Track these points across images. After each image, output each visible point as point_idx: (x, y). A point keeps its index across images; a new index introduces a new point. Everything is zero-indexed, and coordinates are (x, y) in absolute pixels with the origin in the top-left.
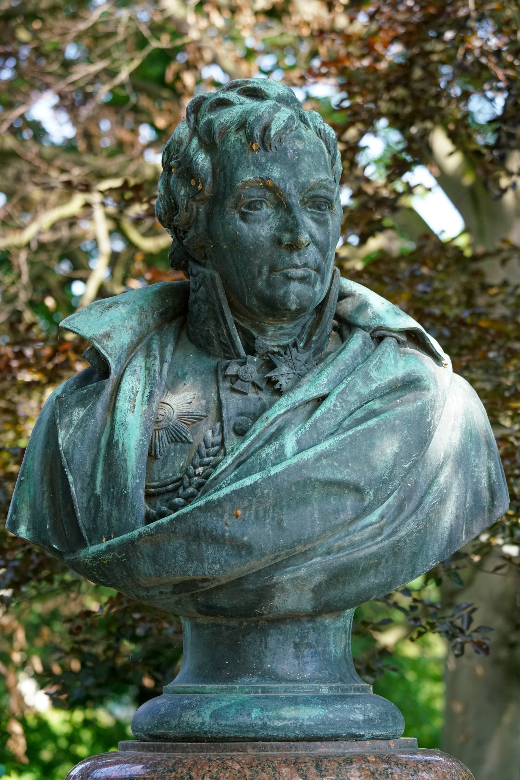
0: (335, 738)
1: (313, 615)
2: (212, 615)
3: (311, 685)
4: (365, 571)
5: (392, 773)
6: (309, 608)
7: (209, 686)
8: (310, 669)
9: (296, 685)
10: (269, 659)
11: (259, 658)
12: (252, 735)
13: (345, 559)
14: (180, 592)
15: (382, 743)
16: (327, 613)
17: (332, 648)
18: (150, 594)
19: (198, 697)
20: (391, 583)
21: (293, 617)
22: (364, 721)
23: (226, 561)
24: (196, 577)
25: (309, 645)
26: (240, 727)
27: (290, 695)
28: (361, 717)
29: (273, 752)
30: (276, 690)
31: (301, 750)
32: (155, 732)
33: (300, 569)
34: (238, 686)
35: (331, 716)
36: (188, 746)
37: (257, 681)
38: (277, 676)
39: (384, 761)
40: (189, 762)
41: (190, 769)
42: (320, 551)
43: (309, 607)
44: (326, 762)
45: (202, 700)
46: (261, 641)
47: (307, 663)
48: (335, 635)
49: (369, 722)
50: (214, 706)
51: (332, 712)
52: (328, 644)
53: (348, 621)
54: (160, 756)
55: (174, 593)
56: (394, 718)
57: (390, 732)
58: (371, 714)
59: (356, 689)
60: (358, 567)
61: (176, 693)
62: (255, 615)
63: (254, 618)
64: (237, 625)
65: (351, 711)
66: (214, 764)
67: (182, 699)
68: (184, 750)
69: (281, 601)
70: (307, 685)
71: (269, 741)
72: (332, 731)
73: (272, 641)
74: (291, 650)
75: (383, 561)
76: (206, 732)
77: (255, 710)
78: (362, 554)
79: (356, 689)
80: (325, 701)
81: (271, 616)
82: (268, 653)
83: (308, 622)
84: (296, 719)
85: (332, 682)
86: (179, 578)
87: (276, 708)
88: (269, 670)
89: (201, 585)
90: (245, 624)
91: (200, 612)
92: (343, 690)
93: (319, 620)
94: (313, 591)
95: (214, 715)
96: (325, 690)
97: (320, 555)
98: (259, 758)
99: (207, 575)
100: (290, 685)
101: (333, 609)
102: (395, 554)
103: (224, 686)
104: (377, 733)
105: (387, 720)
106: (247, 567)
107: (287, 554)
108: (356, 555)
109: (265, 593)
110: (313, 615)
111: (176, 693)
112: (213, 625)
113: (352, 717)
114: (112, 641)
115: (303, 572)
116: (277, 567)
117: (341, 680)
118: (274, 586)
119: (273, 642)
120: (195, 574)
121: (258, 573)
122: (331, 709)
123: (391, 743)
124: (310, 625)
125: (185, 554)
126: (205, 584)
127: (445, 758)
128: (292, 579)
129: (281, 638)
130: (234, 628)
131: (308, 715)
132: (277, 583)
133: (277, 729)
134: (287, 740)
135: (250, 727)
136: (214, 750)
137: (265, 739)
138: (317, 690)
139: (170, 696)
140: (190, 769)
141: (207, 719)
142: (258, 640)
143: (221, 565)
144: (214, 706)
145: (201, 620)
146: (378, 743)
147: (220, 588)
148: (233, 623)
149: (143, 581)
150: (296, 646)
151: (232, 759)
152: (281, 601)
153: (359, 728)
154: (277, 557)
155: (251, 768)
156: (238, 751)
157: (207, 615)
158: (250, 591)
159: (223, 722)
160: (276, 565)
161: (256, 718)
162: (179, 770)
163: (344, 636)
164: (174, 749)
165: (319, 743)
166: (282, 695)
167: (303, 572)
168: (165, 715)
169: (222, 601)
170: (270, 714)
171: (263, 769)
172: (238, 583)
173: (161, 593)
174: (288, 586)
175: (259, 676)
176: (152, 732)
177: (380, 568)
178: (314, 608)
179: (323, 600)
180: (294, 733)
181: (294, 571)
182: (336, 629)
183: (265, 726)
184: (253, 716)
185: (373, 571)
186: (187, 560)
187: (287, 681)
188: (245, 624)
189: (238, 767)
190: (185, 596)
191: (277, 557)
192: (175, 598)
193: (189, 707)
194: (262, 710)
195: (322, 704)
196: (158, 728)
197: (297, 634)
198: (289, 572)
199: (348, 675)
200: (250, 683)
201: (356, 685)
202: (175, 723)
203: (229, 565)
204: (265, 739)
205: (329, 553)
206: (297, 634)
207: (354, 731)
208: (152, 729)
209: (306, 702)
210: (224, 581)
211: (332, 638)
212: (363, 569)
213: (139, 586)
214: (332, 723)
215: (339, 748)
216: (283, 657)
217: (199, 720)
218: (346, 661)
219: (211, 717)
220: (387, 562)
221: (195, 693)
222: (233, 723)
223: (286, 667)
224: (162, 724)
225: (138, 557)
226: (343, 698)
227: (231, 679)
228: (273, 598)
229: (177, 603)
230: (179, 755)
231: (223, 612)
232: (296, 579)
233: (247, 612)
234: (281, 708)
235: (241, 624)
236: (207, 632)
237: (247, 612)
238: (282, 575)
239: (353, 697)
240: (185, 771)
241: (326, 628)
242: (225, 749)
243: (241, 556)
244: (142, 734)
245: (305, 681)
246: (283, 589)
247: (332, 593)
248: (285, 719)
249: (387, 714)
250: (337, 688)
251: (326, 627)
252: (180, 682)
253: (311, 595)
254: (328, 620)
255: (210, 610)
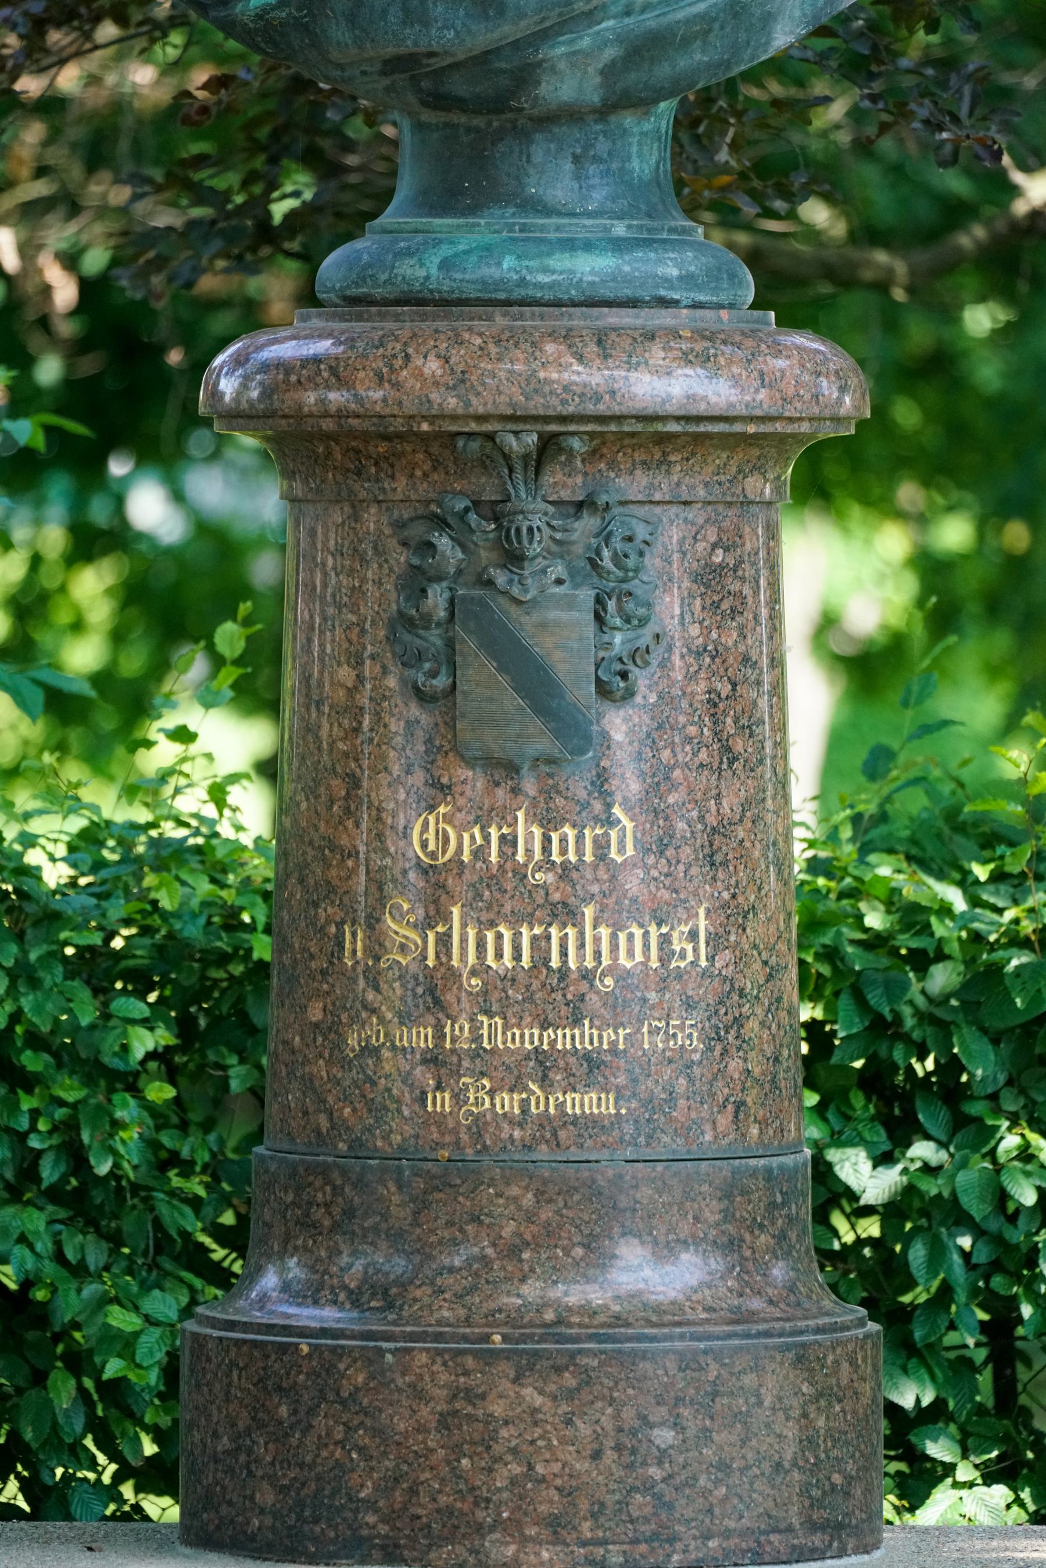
0: (633, 303)
1: (606, 110)
2: (443, 109)
3: (597, 221)
4: (686, 42)
5: (715, 356)
6: (596, 99)
7: (437, 221)
8: (598, 197)
9: (575, 221)
10: (533, 180)
11: (518, 178)
12: (502, 296)
13: (652, 24)
14: (393, 73)
15: (708, 314)
16: (625, 107)
17: (635, 164)
18: (347, 74)
19: (420, 237)
20: (728, 61)
21: (571, 115)
22: (680, 278)
23: (464, 25)
24: (416, 50)
25: (597, 159)
26: (484, 282)
27: (564, 235)
28: (675, 272)
29: (531, 321)
30: (542, 228)
31: (578, 319)
32: (354, 292)
33: (581, 38)
34: (482, 222)
35: (627, 268)
36: (403, 313)
37: (513, 215)
38: (545, 206)
39: (704, 337)
40: (407, 333)
41: (405, 344)
42: (614, 9)
43: (595, 99)
44: (613, 336)
45: (426, 243)
46: (521, 152)
47: (593, 187)
48: (640, 144)
49: (687, 280)
50: (446, 251)
51: (629, 263)
52: (629, 159)
53: (664, 123)
54: (358, 326)
55: (383, 73)
56: (732, 276)
57: (723, 298)
58: (692, 268)
59: (672, 230)
60: (675, 35)
61: (385, 231)
62: (511, 110)
63: (510, 115)
64: (482, 125)
65: (660, 261)
66: (442, 337)
67: (396, 241)
68: (397, 318)
69: (551, 88)
70: (588, 222)
71: (530, 305)
72: (627, 292)
73: (538, 152)
74: (568, 166)
75: (716, 26)
76: (431, 291)
77: (508, 258)
78: (680, 15)
79: (672, 230)
80: (618, 246)
81: (535, 112)
82: (531, 171)
83: (596, 122)
84: (572, 272)
85: (633, 218)
86: (391, 51)
87: (540, 255)
88: (532, 196)
89: (425, 61)
90: (495, 124)
91: (424, 104)
92: (650, 231)
93: (613, 118)
94: (602, 72)
95: (445, 265)
96: (620, 229)
97: (614, 17)
98: (511, 329)
99: (435, 47)
100: (565, 221)
101: (641, 102)
102: (736, 15)
103: (461, 221)
104: (702, 298)
105: (718, 279)
106: (496, 35)
107: (560, 15)
108: (672, 17)
109: (526, 76)
110: (606, 110)
111: (385, 231)
112: (447, 125)
113: (660, 271)
114: (259, 162)
115: (586, 42)
116: (544, 35)
117: (649, 215)
118: (539, 64)
119: (541, 153)
120: (416, 44)
121: (516, 45)
122: (627, 258)
123: (724, 314)
124: (599, 127)
125: (400, 14)
126: (432, 61)
127: (824, 342)
128: (568, 55)
129: (552, 146)
130: (478, 130)
131: (590, 267)
132: (543, 60)
133: (542, 286)
134: (558, 304)
135: (499, 284)
136: (446, 317)
137: (522, 303)
138: (607, 229)
139: (377, 237)
140: (405, 344)
141: (434, 271)
142: (517, 149)
143: (457, 32)
144: (446, 251)
145: (428, 116)
146: (699, 313)
147: (456, 66)
148: (479, 121)
149: (334, 55)
150: (576, 159)
151: (470, 329)
152: (551, 88)
153: (672, 288)
154: (543, 20)
155: (498, 342)
156: (480, 319)
157: (435, 108)
158: (503, 71)
159: (458, 276)
160: (545, 31)
161: (509, 270)
162: (390, 346)
163: (655, 146)
164: (382, 316)
165: (606, 310)
166: (552, 236)
167: (586, 42)
168: (369, 265)
169: (459, 86)
170: (531, 263)
171: (516, 345)
172: (483, 59)
173: (364, 73)
174: (562, 65)
175: (517, 206)
176: (348, 293)
177: (711, 37)
178: (604, 100)
179: (619, 87)
180: (568, 292)
181: (571, 42)
182: (642, 133)
183: (522, 282)
184: (505, 266)
185: (698, 43)
186: (404, 23)
187: (560, 214)
188: (495, 124)
189: (478, 341)
190: (401, 79)
191: (543, 20)
192: (386, 81)
193: (408, 253)
194: (519, 257)
195: (613, 251)
196: (357, 285)
197: (577, 141)
198: (563, 43)
199: (660, 207)
200: (503, 217)
201: (673, 223)
202: (383, 277)
203: (469, 31)
204: (522, 303)
205: (628, 14)
206: (577, 141)
207: (662, 292)
208: (348, 287)
209: (588, 246)
210: (461, 57)
211: (635, 149)
212: (683, 39)
213: (330, 61)
214: (628, 280)
215: (638, 317)
216: (552, 176)
217: (422, 273)
218: (659, 184)
219: (440, 268)
220: (722, 28)
221: (416, 231)
222: (474, 277)
223: (559, 193)
224: (364, 279)
225: (327, 16)
226: (647, 243)
227: (473, 210)
228: (539, 83)
229: (389, 89)
230: (389, 325)
231: (458, 104)
232: (574, 53)
233: (498, 104)
234: (549, 254)
235: (489, 124)
236: (435, 135)
237: (498, 104)
238: (553, 47)
239: (664, 241)
240: (398, 346)
241: (625, 132)
242: (460, 317)
243: (487, 18)
244: (332, 295)
245: (589, 215)
246: (553, 70)
247: (633, 76)
248: (553, 272)
249: (719, 269)
250: (640, 227)
251: (625, 130)
252: (393, 216)
253: (598, 80)
254: (628, 120)
255: (440, 101)
